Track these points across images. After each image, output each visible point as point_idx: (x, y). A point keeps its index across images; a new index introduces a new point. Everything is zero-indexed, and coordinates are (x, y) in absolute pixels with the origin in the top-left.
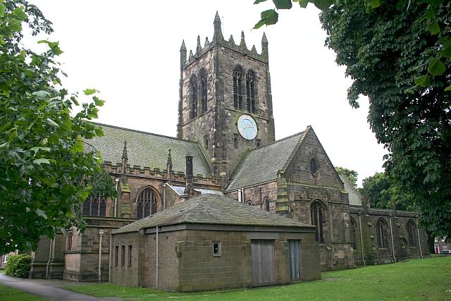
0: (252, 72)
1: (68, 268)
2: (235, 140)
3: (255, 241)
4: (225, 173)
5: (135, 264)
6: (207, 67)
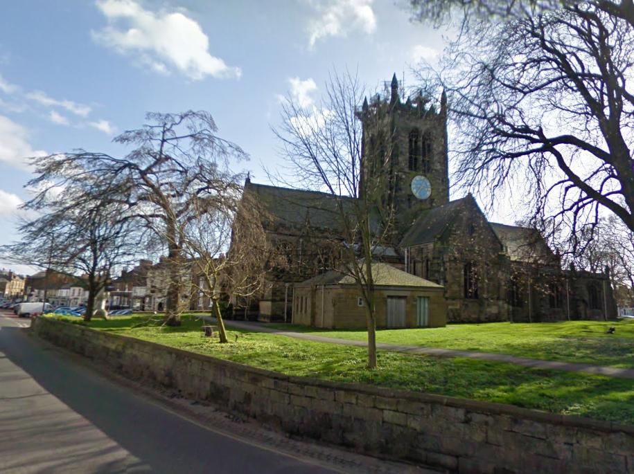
0: (428, 133)
1: (262, 312)
2: (409, 200)
3: (392, 297)
4: (397, 232)
5: (309, 310)
6: (385, 129)
